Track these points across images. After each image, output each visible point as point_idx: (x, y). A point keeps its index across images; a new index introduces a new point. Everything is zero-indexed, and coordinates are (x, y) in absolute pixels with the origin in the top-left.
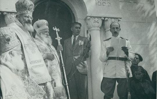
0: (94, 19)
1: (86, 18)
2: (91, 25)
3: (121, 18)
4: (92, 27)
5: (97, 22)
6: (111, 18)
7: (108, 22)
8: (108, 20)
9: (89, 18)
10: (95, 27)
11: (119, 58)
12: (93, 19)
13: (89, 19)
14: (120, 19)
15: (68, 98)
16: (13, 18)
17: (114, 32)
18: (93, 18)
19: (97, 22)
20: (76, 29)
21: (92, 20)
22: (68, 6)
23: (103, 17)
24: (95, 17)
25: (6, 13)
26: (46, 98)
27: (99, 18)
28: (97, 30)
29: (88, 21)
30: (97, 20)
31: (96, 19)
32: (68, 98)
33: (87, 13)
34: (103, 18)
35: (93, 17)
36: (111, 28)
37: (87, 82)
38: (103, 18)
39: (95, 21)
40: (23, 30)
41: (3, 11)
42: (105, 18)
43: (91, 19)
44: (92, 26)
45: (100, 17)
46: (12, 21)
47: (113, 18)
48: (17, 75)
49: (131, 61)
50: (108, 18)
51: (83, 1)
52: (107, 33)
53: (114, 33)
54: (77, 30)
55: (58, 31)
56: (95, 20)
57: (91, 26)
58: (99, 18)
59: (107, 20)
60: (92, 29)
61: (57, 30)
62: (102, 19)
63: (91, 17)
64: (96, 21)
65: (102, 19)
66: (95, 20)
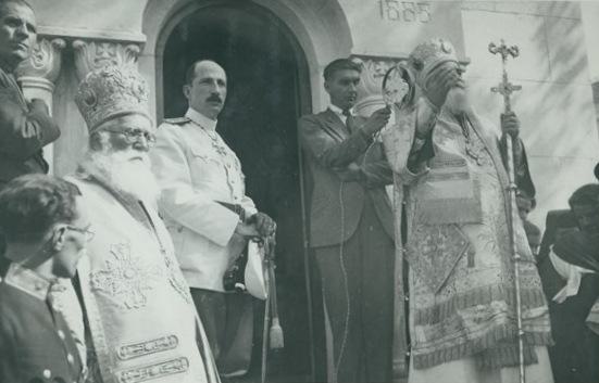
3: (375, 76)
4: (368, 92)
12: (372, 66)
15: (209, 381)
17: (209, 95)
20: (340, 87)
26: (47, 380)
27: (119, 46)
32: (209, 381)
33: (351, 46)
34: (62, 43)
38: (62, 43)
39: (378, 71)
40: (432, 70)
43: (366, 65)
51: (338, 4)
53: (209, 100)
54: (344, 89)
56: (378, 67)
60: (369, 98)
63: (366, 58)
66: (100, 49)
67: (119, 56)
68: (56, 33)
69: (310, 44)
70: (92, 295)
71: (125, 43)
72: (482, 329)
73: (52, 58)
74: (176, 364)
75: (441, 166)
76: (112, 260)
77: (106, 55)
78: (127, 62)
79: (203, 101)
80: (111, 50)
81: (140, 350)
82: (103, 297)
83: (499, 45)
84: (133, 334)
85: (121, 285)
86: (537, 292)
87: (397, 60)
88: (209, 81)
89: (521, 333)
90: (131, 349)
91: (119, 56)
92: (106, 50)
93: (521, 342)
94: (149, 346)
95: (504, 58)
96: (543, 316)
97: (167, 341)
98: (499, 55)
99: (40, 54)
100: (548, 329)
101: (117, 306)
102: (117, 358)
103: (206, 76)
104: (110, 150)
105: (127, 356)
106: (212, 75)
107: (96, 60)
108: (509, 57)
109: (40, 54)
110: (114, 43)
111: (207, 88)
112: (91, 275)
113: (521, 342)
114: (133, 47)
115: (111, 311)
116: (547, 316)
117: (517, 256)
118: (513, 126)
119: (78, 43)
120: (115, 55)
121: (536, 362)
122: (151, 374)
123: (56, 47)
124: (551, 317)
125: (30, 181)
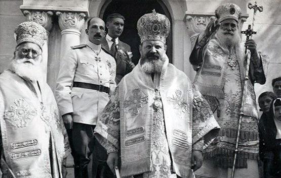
1: (185, 17)
3: (198, 24)
9: (190, 17)
11: (98, 90)
12: (196, 19)
13: (190, 20)
14: (244, 19)
16: (69, 20)
18: (195, 17)
19: (202, 24)
21: (195, 21)
24: (199, 16)
25: (59, 13)
29: (188, 23)
36: (90, 27)
37: (55, 146)
38: (51, 13)
39: (199, 22)
41: (55, 9)
45: (46, 11)
46: (68, 25)
53: (95, 36)
57: (194, 31)
63: (193, 16)
64: (202, 22)
66: (68, 16)
67: (76, 18)
68: (81, 10)
69: (170, 6)
70: (4, 121)
71: (79, 12)
72: (212, 148)
73: (47, 20)
74: (36, 152)
75: (209, 68)
76: (14, 106)
77: (70, 18)
78: (80, 21)
79: (93, 36)
80: (72, 16)
81: (21, 145)
82: (9, 122)
83: (253, 5)
84: (20, 138)
85: (16, 116)
86: (255, 134)
87: (209, 16)
88: (96, 27)
89: (236, 150)
90: (17, 145)
91: (76, 18)
92: (70, 16)
93: (236, 155)
94: (25, 144)
95: (255, 11)
96: (256, 145)
97: (33, 142)
98: (253, 10)
99: (41, 18)
100: (257, 152)
101: (13, 126)
102: (12, 148)
103: (94, 25)
104: (18, 58)
105: (15, 148)
106: (97, 24)
107: (66, 21)
108: (258, 11)
109: (41, 18)
110: (73, 12)
111: (94, 30)
112: (4, 113)
113: (236, 155)
114: (82, 14)
115: (11, 128)
116: (258, 145)
117: (242, 113)
118: (252, 46)
119: (58, 13)
120: (74, 18)
121: (246, 167)
122: (25, 156)
123: (49, 15)
124: (260, 147)
125: (273, 92)
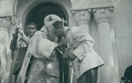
0: (79, 13)
2: (77, 19)
5: (103, 13)
6: (100, 8)
7: (96, 13)
8: (96, 11)
10: (81, 21)
19: (103, 13)
21: (77, 14)
22: (46, 3)
23: (89, 9)
28: (84, 23)
30: (83, 13)
31: (82, 13)
34: (90, 10)
35: (79, 11)
38: (90, 10)
39: (101, 12)
42: (92, 9)
44: (78, 20)
45: (87, 10)
47: (103, 8)
48: (44, 38)
49: (81, 50)
50: (96, 9)
52: (99, 25)
55: (64, 23)
56: (80, 13)
58: (86, 11)
59: (95, 11)
61: (63, 22)
62: (89, 12)
65: (89, 12)
